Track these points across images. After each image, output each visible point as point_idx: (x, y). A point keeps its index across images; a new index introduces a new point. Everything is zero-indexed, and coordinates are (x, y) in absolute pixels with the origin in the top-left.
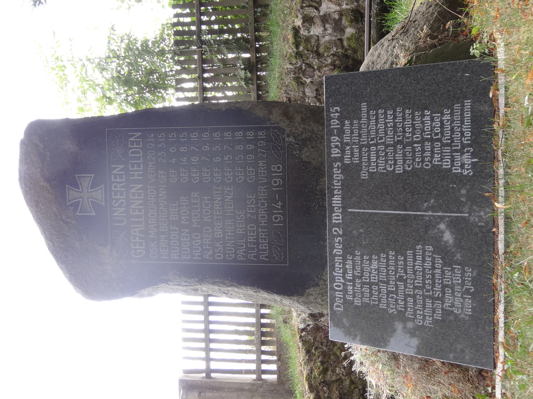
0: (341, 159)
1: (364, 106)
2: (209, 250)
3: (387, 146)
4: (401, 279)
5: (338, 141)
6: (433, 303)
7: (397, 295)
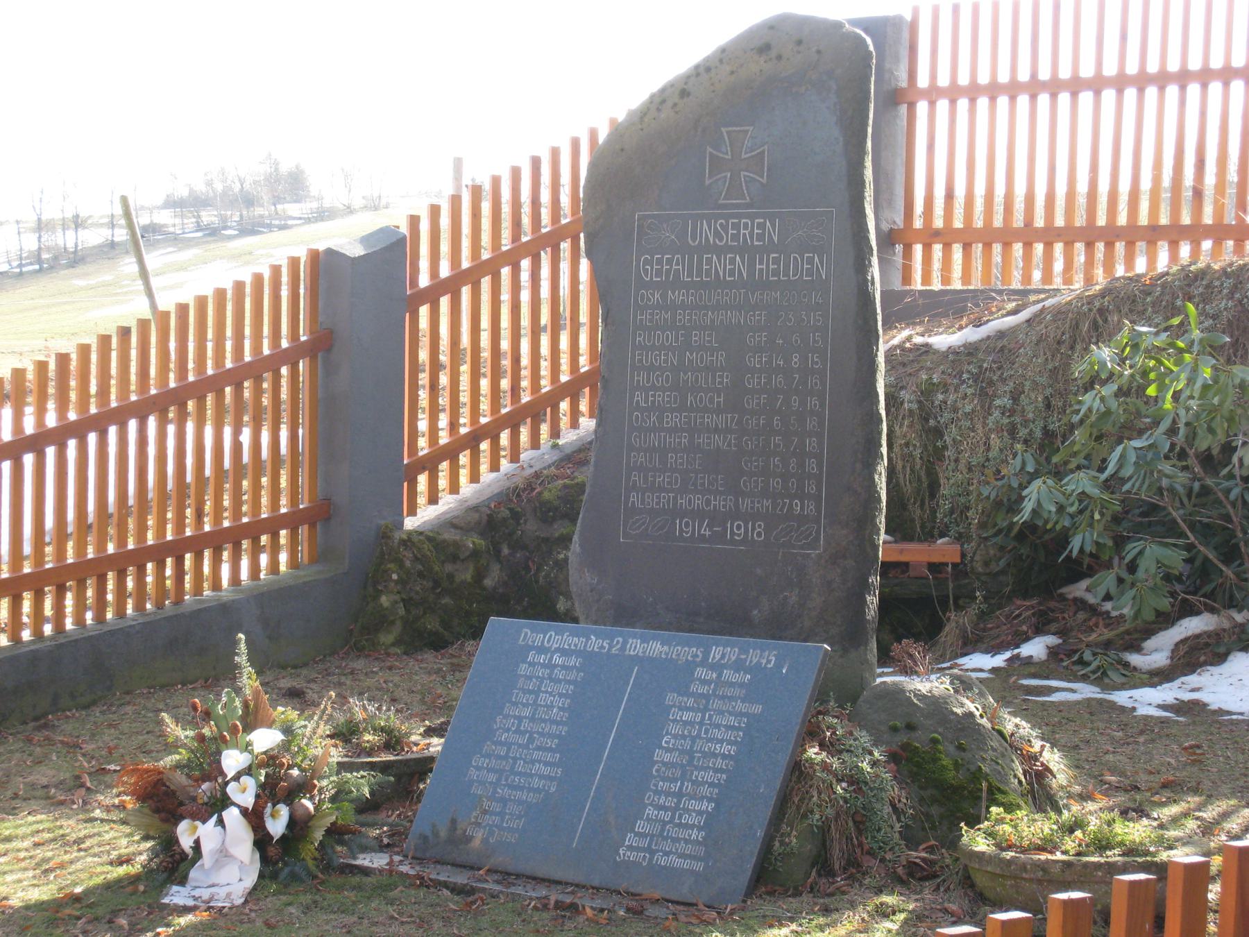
0: (704, 664)
1: (757, 709)
2: (646, 402)
3: (693, 739)
4: (531, 740)
5: (729, 659)
6: (491, 783)
7: (515, 732)
